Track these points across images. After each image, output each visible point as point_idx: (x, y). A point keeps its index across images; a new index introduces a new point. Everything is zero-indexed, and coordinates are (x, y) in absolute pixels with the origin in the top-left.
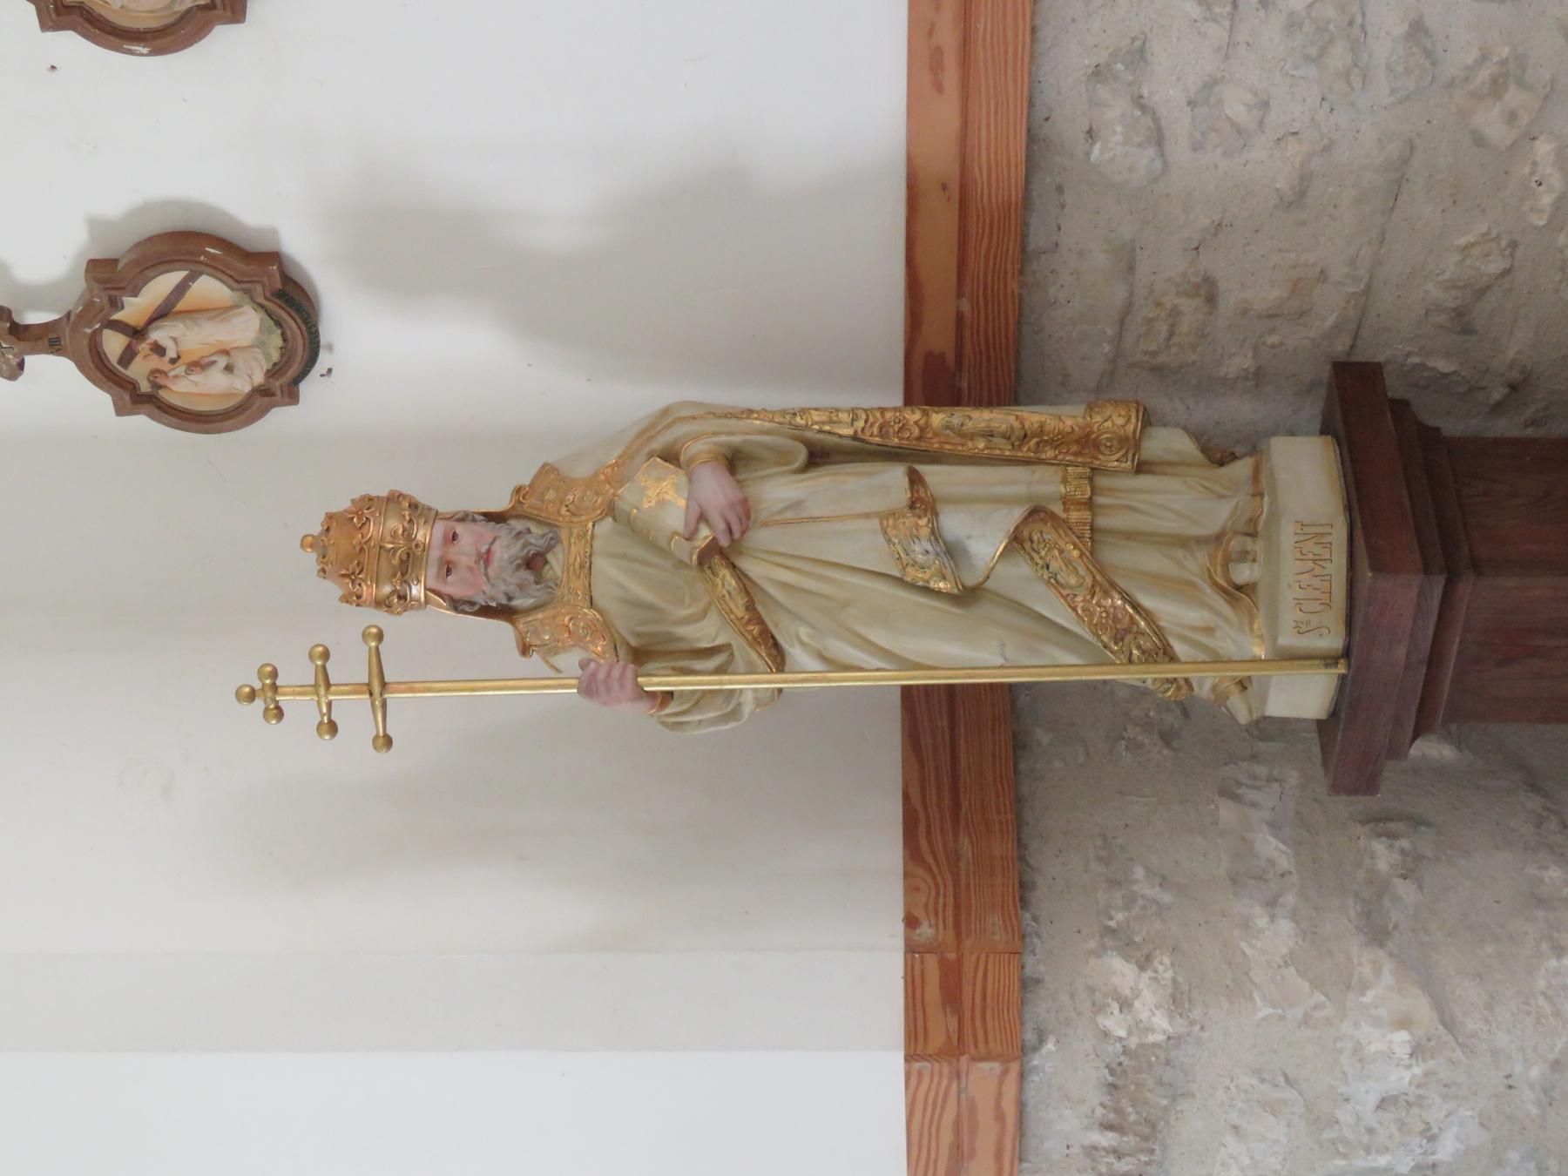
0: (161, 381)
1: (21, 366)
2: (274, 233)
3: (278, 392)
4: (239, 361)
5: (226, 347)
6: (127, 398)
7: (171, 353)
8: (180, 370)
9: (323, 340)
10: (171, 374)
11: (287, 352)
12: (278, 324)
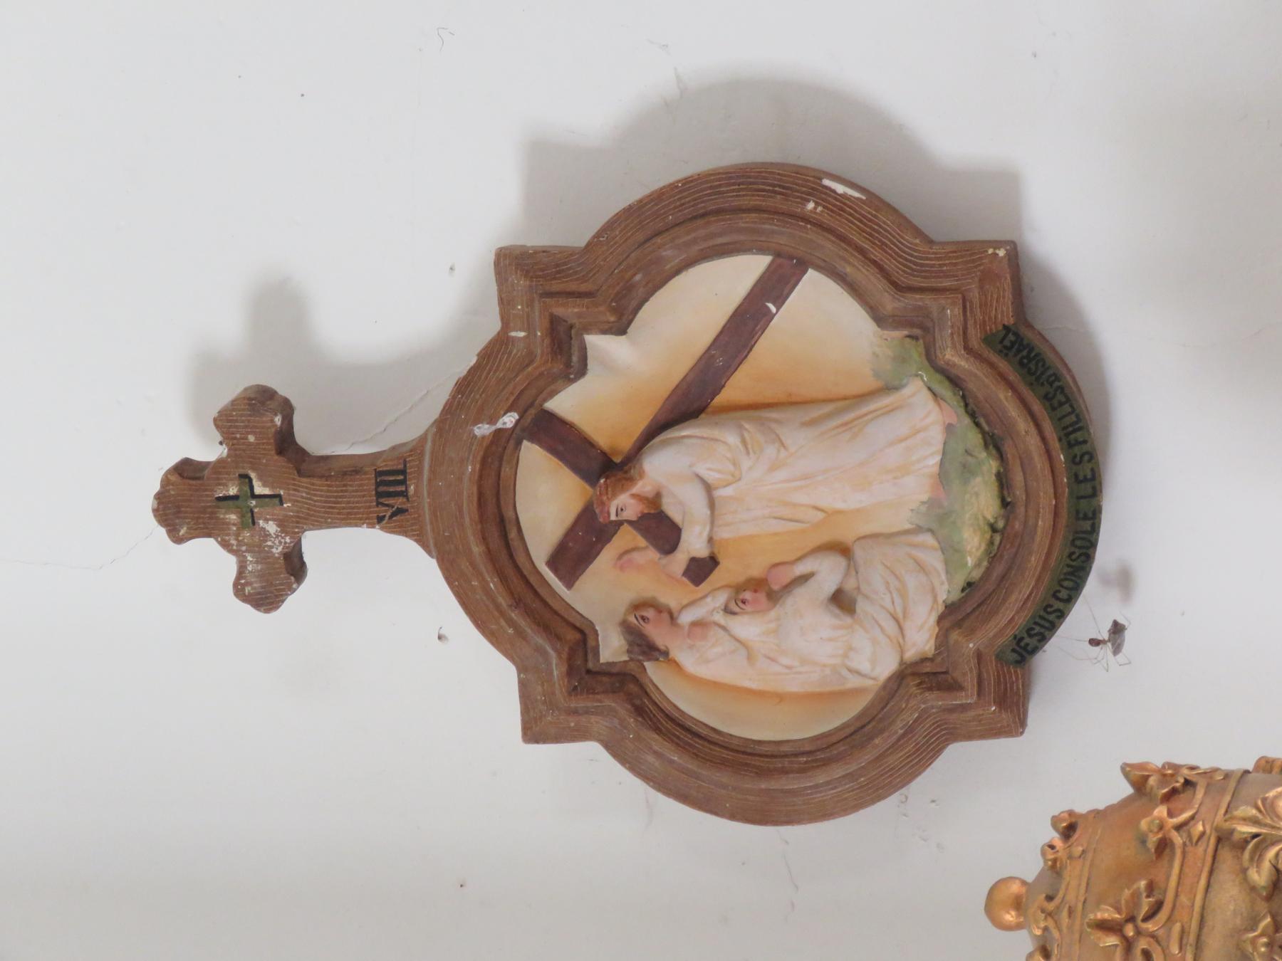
0: (657, 634)
1: (295, 567)
2: (1004, 186)
3: (970, 681)
4: (875, 577)
5: (846, 534)
6: (558, 670)
7: (694, 543)
8: (711, 603)
9: (1105, 556)
10: (686, 618)
11: (1005, 539)
12: (993, 442)
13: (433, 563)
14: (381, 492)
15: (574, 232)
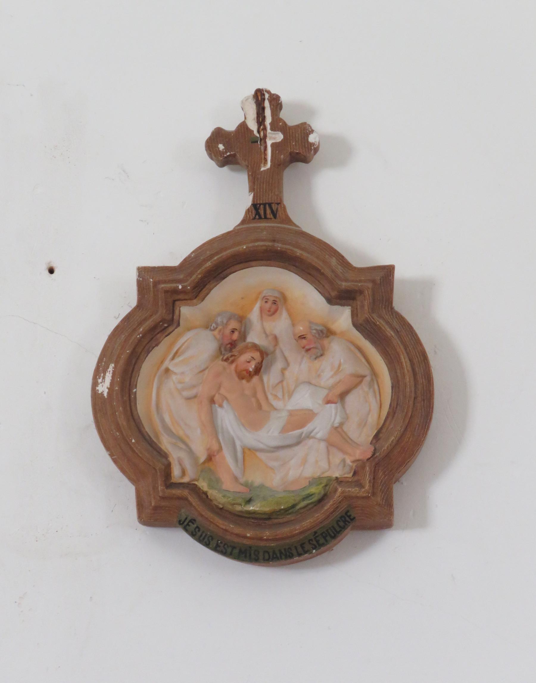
2: (421, 521)
13: (231, 229)
14: (266, 208)
15: (401, 303)
